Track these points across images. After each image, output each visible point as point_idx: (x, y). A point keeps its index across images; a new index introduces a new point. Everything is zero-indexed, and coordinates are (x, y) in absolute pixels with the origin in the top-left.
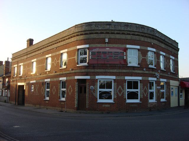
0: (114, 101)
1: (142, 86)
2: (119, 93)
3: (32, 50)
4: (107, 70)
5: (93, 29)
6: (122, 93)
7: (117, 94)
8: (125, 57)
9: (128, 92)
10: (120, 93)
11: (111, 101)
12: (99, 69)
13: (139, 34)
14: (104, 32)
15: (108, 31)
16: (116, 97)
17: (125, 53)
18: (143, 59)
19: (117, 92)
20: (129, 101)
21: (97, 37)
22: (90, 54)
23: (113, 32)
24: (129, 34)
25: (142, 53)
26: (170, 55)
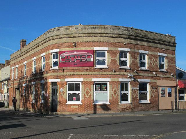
0: (109, 103)
1: (84, 89)
2: (86, 95)
3: (25, 50)
4: (75, 73)
5: (62, 33)
6: (89, 94)
7: (85, 95)
8: (92, 59)
9: (69, 93)
10: (87, 95)
11: (79, 102)
12: (68, 72)
13: (107, 35)
14: (72, 36)
15: (75, 35)
16: (84, 98)
17: (92, 55)
18: (112, 60)
19: (84, 94)
20: (69, 102)
21: (66, 41)
22: (60, 58)
23: (80, 35)
24: (97, 36)
25: (111, 54)
26: (157, 52)
